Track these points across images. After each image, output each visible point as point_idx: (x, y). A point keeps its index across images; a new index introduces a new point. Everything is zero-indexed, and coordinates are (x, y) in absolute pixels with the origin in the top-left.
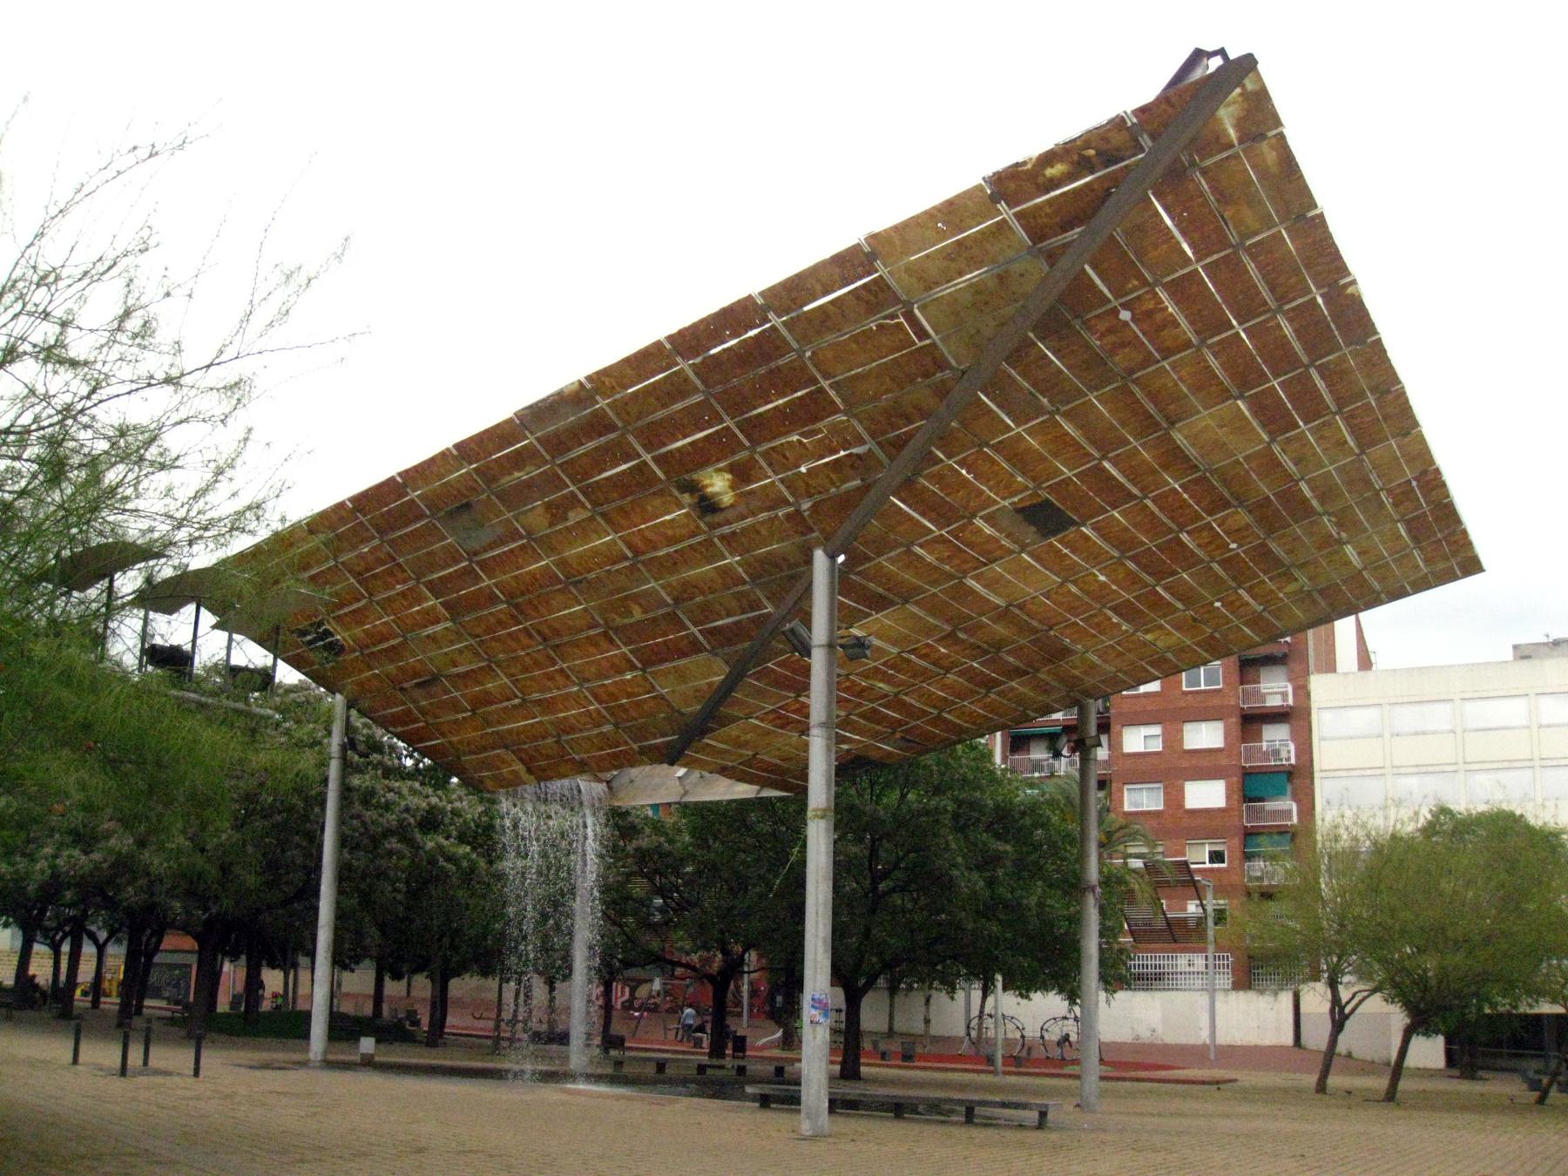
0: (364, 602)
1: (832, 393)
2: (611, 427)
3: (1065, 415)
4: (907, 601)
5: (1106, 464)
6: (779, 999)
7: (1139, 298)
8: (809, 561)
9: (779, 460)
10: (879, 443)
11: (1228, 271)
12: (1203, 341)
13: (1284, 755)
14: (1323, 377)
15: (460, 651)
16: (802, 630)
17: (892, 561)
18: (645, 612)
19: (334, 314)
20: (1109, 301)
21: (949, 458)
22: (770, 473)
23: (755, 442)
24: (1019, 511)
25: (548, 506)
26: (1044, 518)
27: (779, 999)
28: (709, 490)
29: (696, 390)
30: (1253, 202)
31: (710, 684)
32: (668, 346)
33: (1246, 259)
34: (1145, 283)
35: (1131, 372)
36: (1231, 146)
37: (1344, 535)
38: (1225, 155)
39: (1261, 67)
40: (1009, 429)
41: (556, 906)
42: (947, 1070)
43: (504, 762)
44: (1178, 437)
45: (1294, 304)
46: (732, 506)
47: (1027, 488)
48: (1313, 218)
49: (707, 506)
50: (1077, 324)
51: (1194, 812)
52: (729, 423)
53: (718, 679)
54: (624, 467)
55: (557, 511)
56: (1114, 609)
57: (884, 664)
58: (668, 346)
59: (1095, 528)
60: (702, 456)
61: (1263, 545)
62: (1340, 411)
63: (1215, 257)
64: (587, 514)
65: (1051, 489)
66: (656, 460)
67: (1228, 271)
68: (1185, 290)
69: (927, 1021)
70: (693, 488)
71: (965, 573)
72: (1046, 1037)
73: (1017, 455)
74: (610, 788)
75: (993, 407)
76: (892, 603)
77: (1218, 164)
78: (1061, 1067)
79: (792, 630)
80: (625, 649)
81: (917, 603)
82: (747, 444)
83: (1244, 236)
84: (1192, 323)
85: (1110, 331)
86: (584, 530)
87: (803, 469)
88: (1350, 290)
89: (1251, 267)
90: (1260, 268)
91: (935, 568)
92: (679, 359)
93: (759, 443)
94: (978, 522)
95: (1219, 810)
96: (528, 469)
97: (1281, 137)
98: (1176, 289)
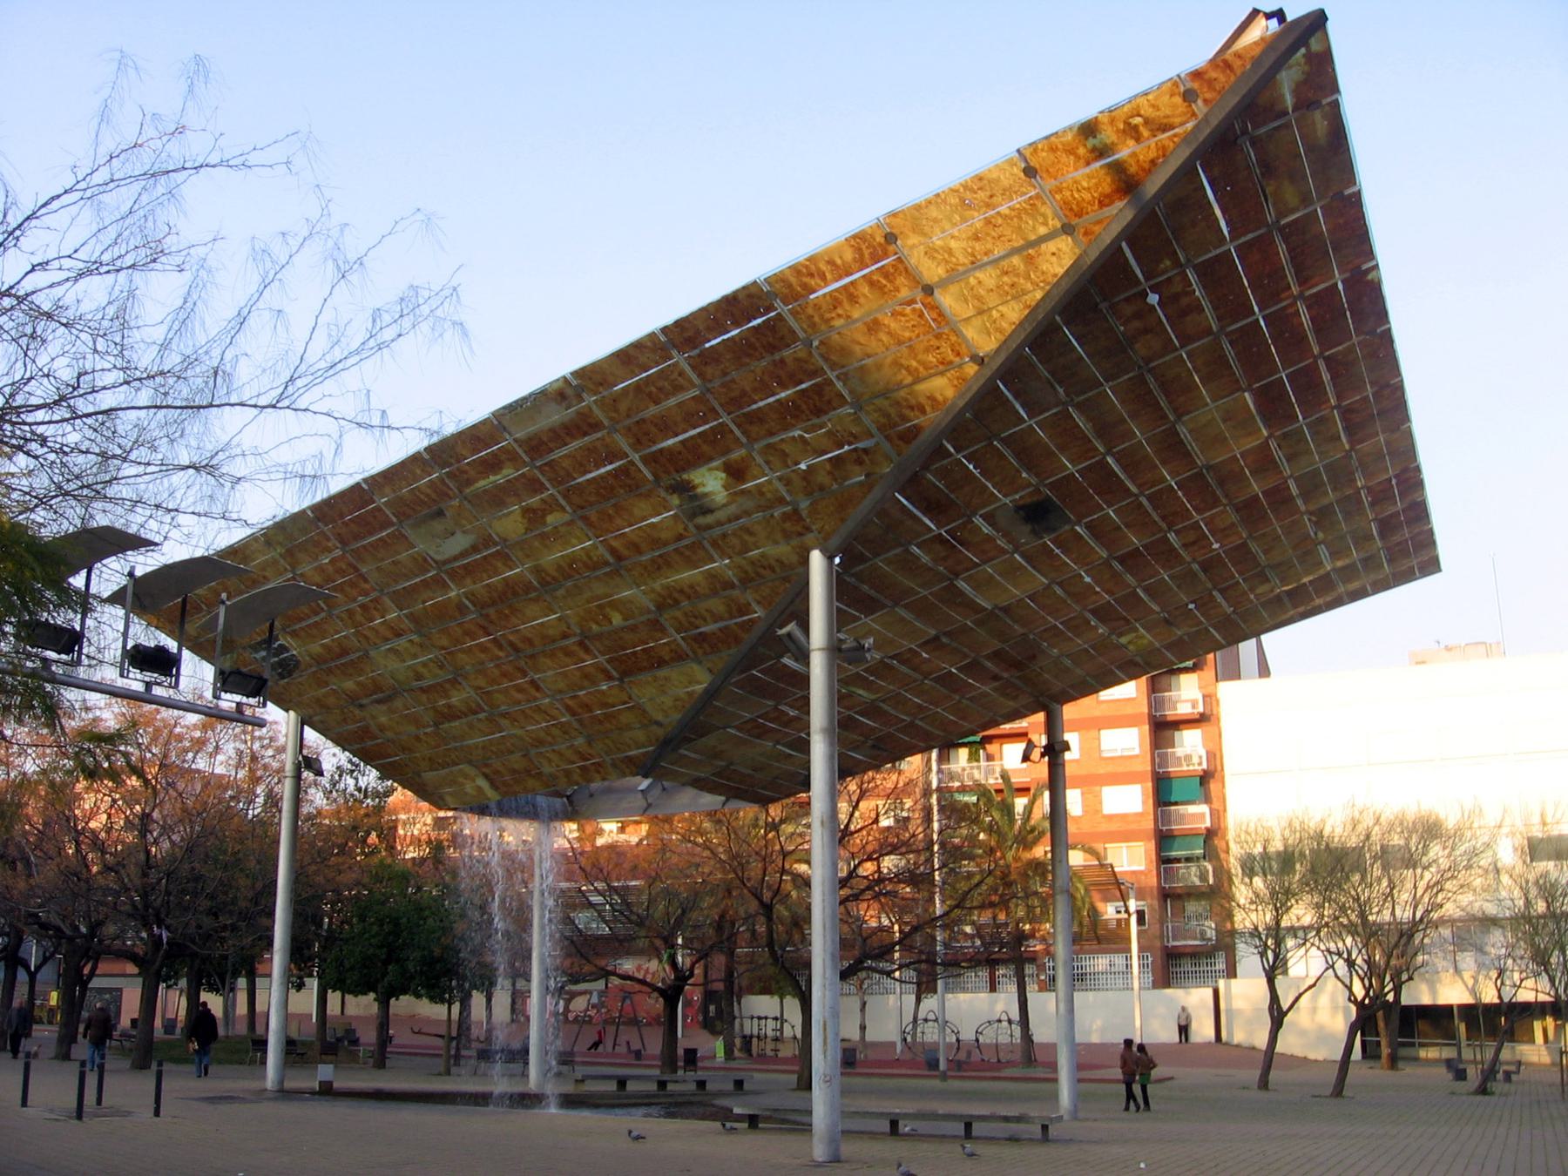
0: (323, 615)
1: (839, 385)
2: (596, 426)
3: (1078, 407)
4: (896, 604)
5: (1110, 460)
6: (712, 1008)
7: (1169, 279)
8: (805, 562)
9: (778, 455)
10: (887, 437)
11: (1258, 252)
12: (1222, 328)
13: (1195, 760)
14: (1329, 369)
15: (424, 664)
16: (798, 633)
17: (889, 562)
18: (625, 619)
19: (382, 286)
20: (1138, 282)
21: (958, 451)
22: (767, 471)
23: (752, 440)
24: (1019, 508)
25: (526, 511)
26: (1037, 514)
27: (712, 1008)
28: (700, 490)
29: (693, 385)
30: (1296, 176)
31: (690, 694)
32: (663, 338)
33: (1278, 239)
34: (1177, 263)
35: (1148, 360)
36: (1286, 113)
37: (1321, 535)
38: (1276, 124)
39: (1330, 25)
40: (1022, 420)
41: (522, 921)
42: (872, 1075)
43: (466, 776)
44: (1182, 430)
45: (1315, 290)
46: (724, 505)
47: (1030, 485)
48: (1351, 196)
49: (697, 506)
50: (1103, 306)
51: (1111, 817)
52: (725, 419)
53: (699, 688)
54: (609, 467)
55: (534, 517)
56: (1094, 612)
57: (865, 671)
58: (663, 338)
59: (1089, 527)
60: (694, 455)
61: (1244, 544)
62: (1109, 452)
63: (1250, 236)
64: (567, 517)
65: (1052, 486)
66: (645, 460)
67: (1258, 252)
68: (1216, 274)
69: (863, 1028)
70: (685, 489)
71: (957, 575)
72: (981, 1039)
73: (1027, 452)
74: (571, 802)
75: (1010, 397)
76: (884, 606)
77: (1269, 135)
78: (999, 1070)
79: (789, 635)
80: (601, 659)
81: (906, 607)
82: (744, 440)
83: (1281, 214)
84: (1215, 308)
85: (1138, 315)
86: (558, 536)
87: (803, 466)
88: (1370, 277)
89: (1282, 250)
90: (1290, 250)
91: (930, 569)
92: (674, 353)
93: (756, 440)
94: (978, 520)
95: (1137, 814)
96: (505, 472)
97: (1336, 105)
98: (1204, 271)
